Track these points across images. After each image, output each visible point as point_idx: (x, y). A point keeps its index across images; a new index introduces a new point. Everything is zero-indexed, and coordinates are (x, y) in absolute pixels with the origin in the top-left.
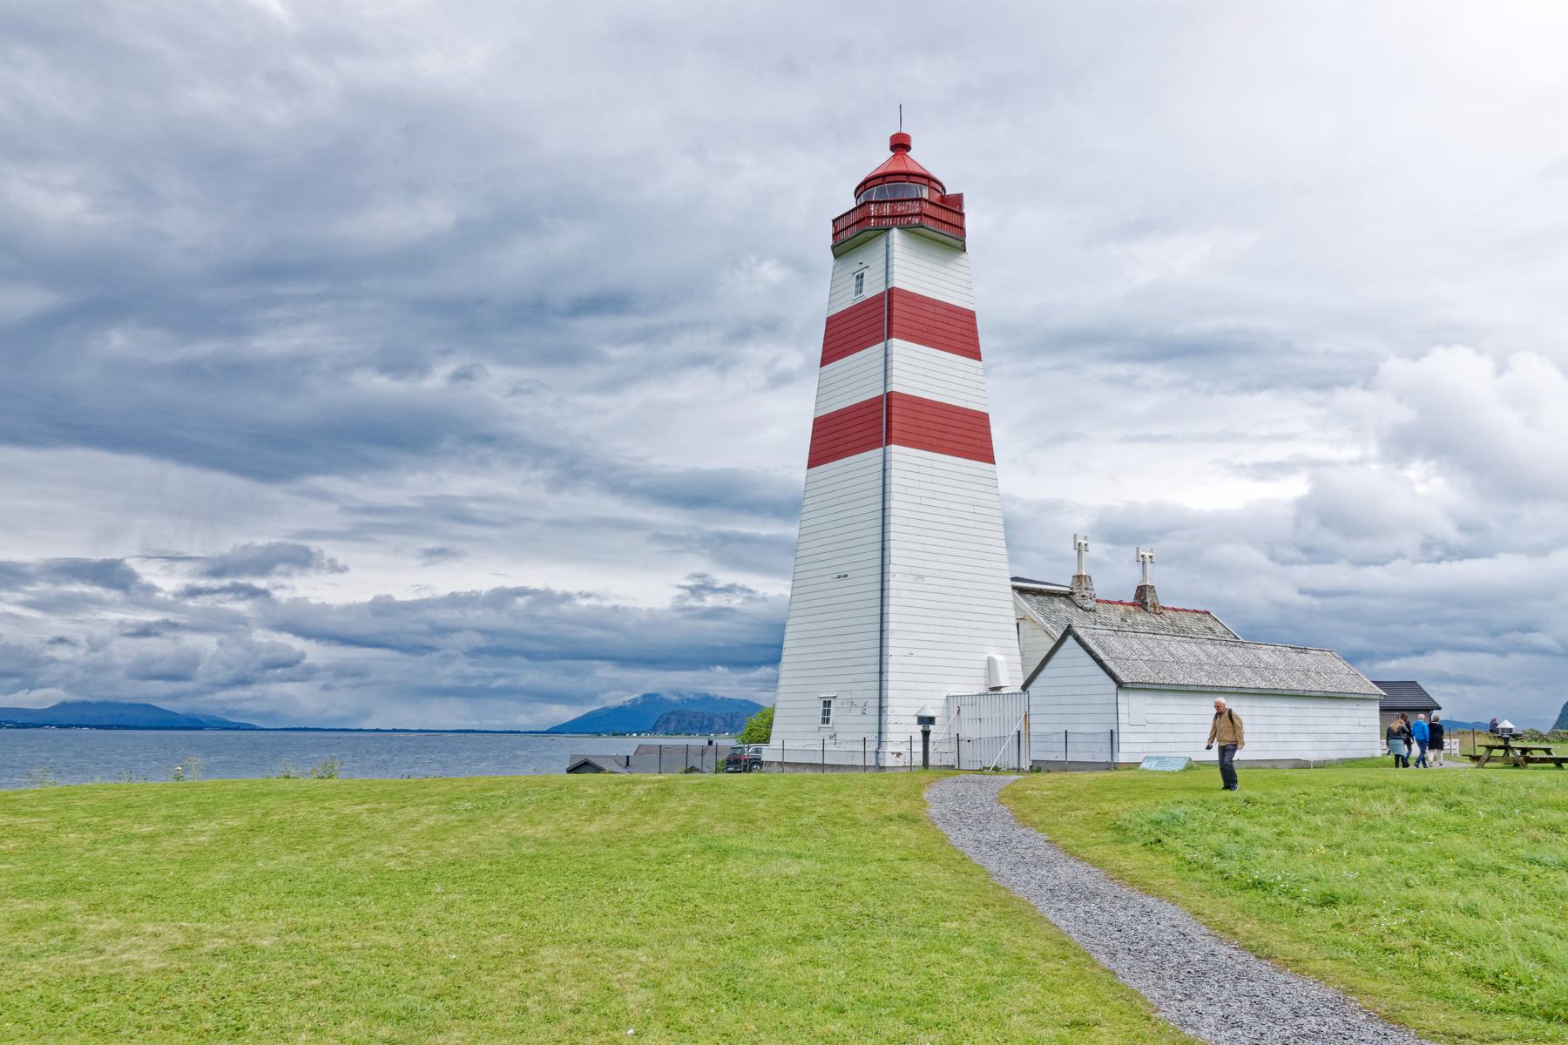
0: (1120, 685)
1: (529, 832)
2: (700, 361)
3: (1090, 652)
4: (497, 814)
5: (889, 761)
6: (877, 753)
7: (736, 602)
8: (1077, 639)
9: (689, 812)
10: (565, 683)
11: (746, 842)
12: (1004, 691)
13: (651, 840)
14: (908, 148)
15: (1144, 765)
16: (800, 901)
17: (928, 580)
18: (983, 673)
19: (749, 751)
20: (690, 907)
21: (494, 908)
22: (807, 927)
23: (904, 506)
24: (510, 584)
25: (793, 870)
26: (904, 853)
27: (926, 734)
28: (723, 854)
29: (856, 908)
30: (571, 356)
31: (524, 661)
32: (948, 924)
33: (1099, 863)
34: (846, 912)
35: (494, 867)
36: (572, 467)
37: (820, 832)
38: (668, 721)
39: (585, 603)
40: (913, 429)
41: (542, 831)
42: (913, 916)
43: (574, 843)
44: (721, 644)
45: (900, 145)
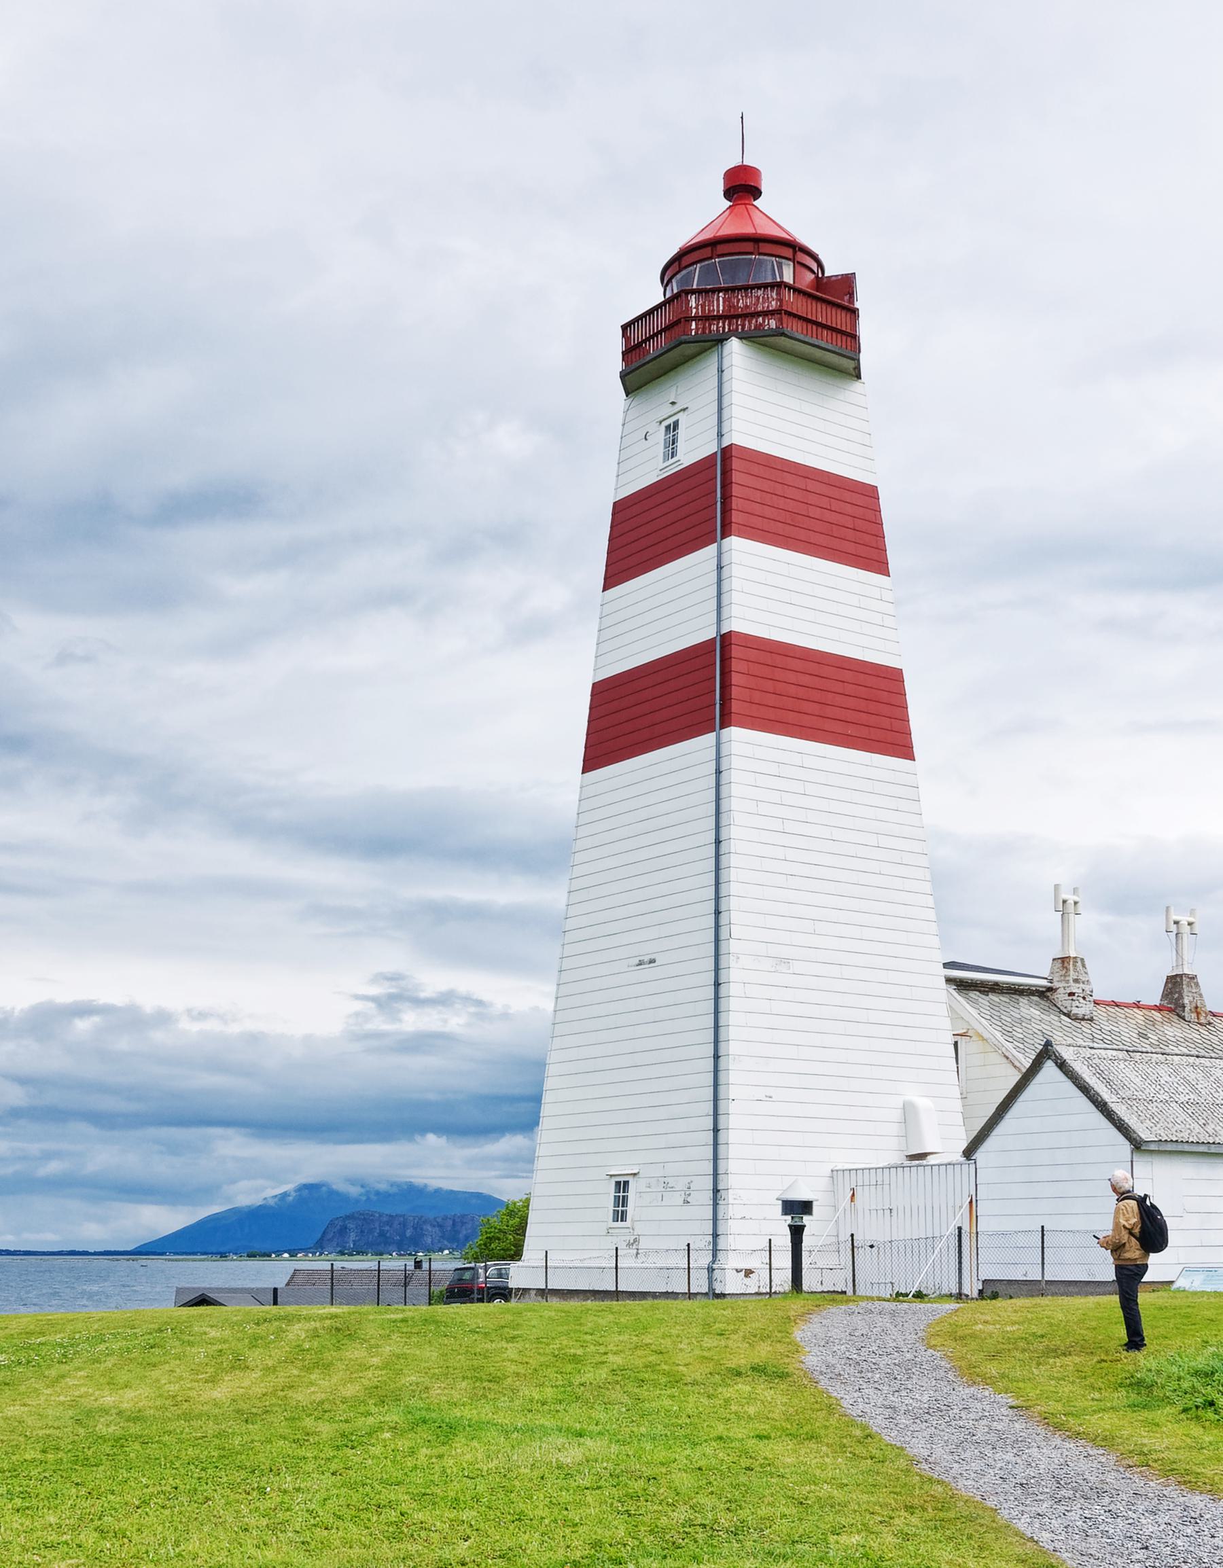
0: (1138, 1145)
1: (108, 1400)
2: (394, 597)
3: (1085, 1089)
4: (53, 1373)
5: (731, 1283)
6: (711, 1270)
7: (455, 1022)
8: (1062, 1065)
9: (385, 1366)
10: (163, 1168)
11: (484, 1412)
12: (931, 1160)
13: (321, 1410)
14: (756, 193)
15: (1181, 1283)
16: (580, 1504)
18: (894, 1129)
19: (487, 1273)
20: (393, 1515)
21: (53, 1519)
22: (597, 1545)
24: (65, 996)
25: (572, 1455)
26: (764, 1427)
27: (797, 1232)
28: (448, 1431)
29: (681, 1514)
30: (158, 596)
31: (92, 1130)
32: (844, 1539)
33: (1106, 1441)
34: (664, 1521)
35: (50, 1457)
36: (164, 790)
37: (616, 1394)
38: (343, 1231)
39: (195, 1027)
40: (771, 700)
41: (128, 1399)
42: (783, 1526)
43: (187, 1417)
44: (432, 1097)
45: (742, 186)
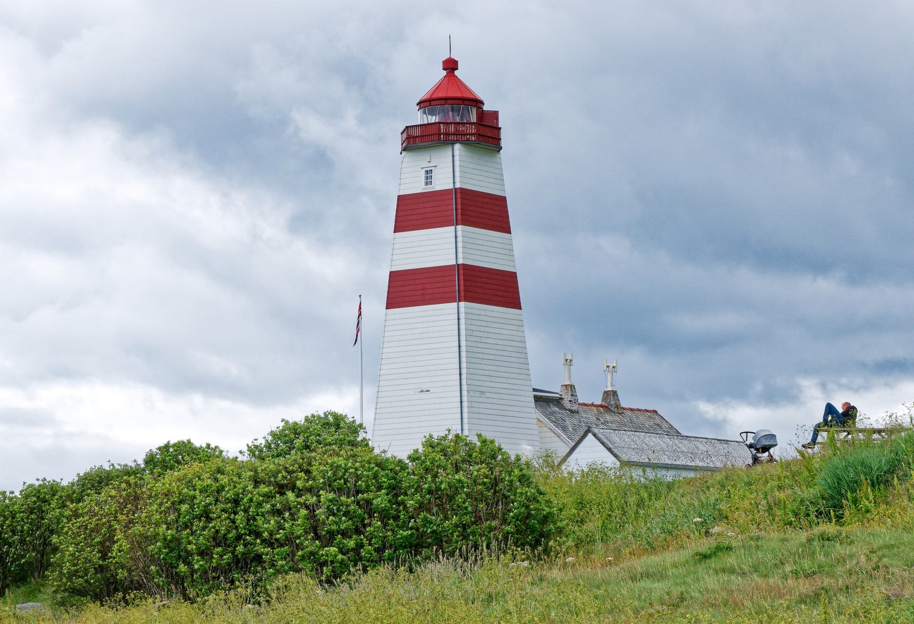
17: (487, 395)
23: (523, 393)
45: (451, 65)
